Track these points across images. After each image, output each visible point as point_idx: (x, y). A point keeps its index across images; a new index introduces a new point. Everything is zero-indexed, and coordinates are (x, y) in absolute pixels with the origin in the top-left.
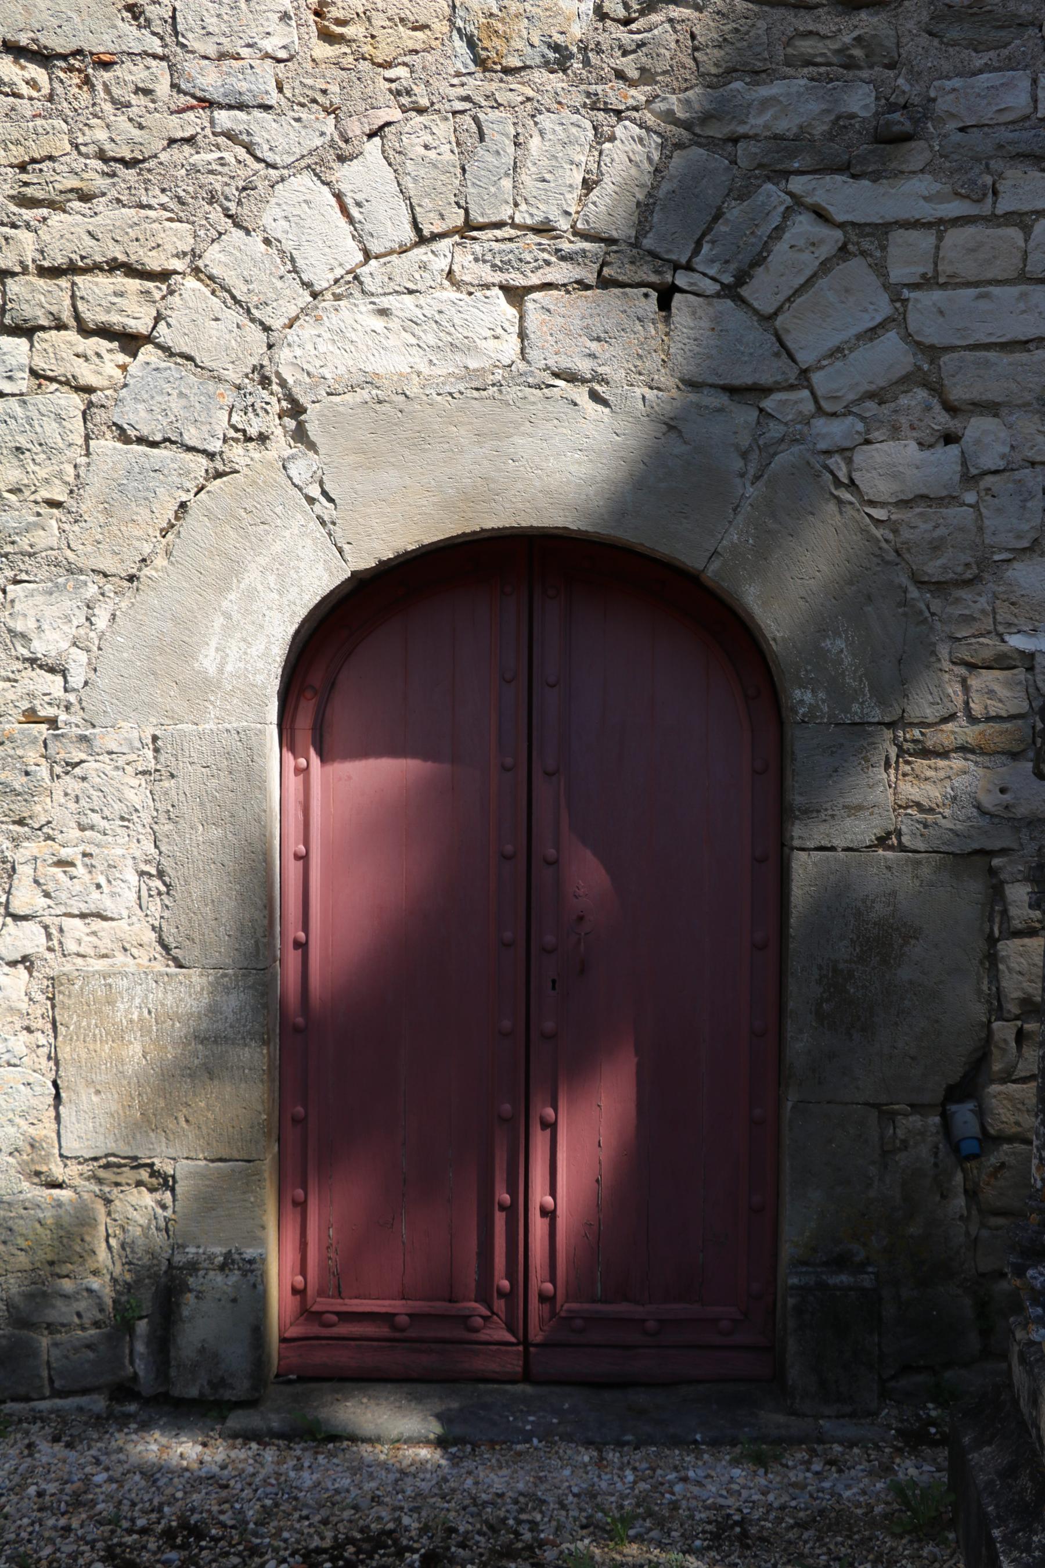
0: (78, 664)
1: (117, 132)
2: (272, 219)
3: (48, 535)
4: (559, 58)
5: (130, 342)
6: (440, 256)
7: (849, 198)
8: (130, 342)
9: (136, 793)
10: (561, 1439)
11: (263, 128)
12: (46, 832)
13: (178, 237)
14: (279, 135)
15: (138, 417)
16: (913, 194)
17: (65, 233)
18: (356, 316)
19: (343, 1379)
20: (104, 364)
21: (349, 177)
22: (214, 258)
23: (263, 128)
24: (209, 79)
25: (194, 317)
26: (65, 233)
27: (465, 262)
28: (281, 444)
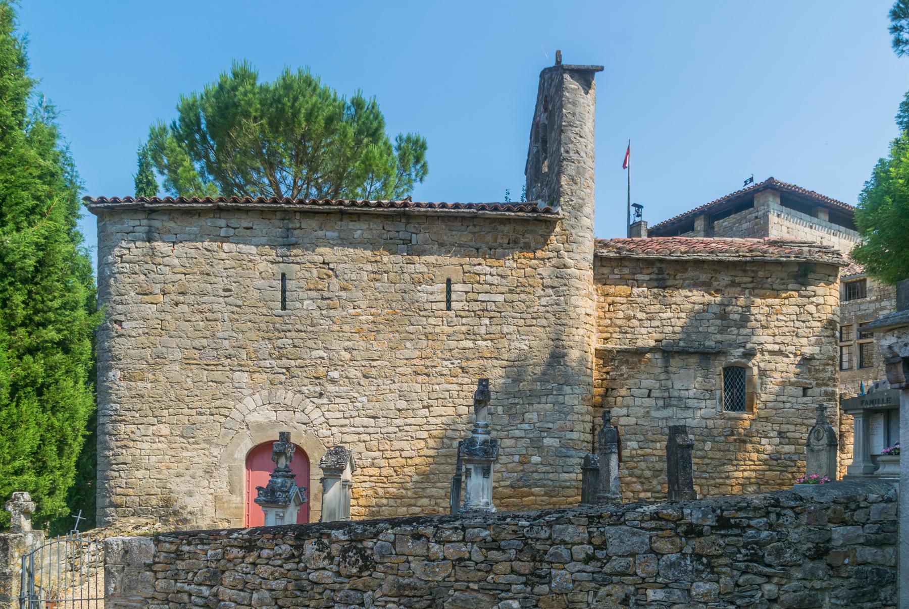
0: (219, 456)
1: (224, 391)
2: (245, 402)
3: (215, 440)
4: (281, 383)
5: (226, 417)
6: (266, 407)
7: (317, 401)
8: (226, 417)
9: (226, 473)
10: (7, 565)
11: (244, 391)
12: (214, 477)
13: (233, 404)
14: (245, 392)
15: (227, 426)
16: (324, 400)
17: (218, 403)
18: (255, 414)
19: (463, 218)
20: (223, 419)
21: (254, 397)
22: (237, 406)
23: (244, 391)
24: (237, 385)
25: (235, 414)
26: (218, 403)
27: (269, 407)
28: (246, 429)
